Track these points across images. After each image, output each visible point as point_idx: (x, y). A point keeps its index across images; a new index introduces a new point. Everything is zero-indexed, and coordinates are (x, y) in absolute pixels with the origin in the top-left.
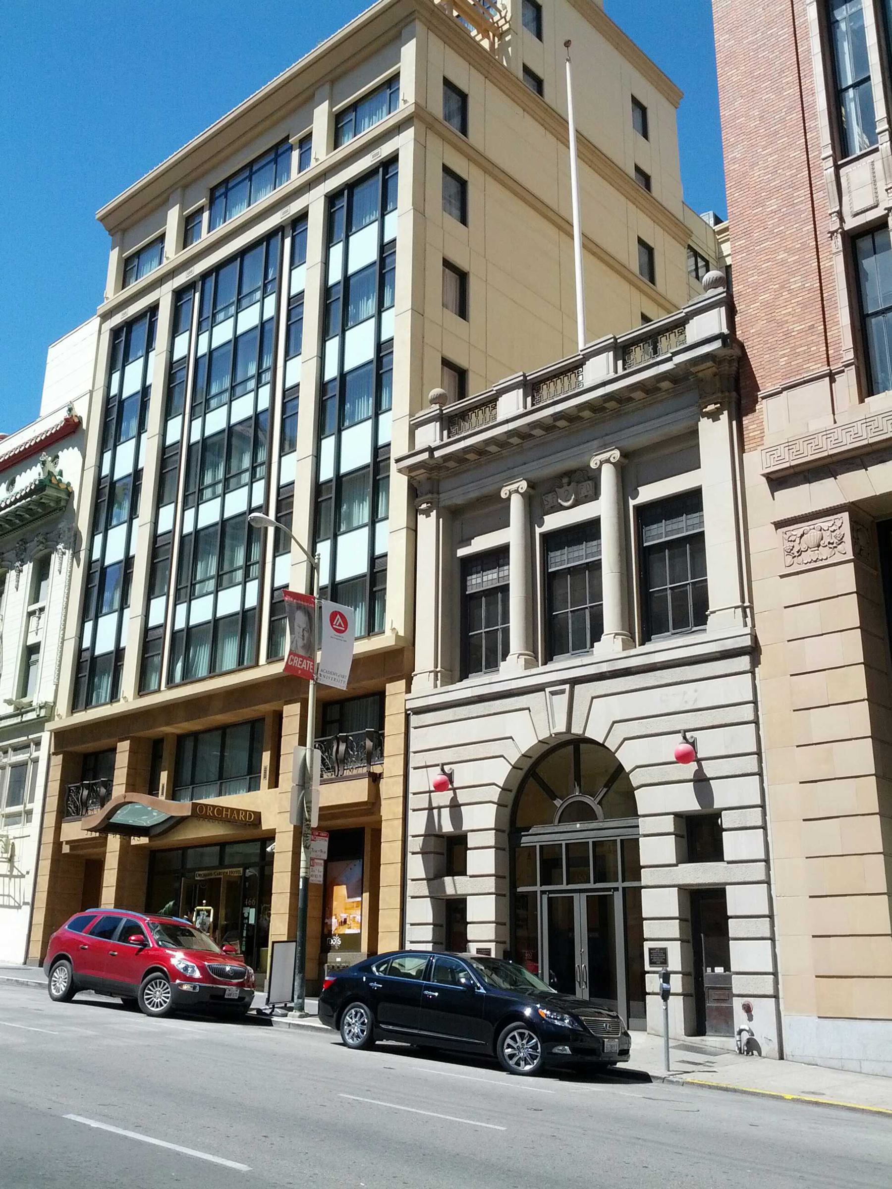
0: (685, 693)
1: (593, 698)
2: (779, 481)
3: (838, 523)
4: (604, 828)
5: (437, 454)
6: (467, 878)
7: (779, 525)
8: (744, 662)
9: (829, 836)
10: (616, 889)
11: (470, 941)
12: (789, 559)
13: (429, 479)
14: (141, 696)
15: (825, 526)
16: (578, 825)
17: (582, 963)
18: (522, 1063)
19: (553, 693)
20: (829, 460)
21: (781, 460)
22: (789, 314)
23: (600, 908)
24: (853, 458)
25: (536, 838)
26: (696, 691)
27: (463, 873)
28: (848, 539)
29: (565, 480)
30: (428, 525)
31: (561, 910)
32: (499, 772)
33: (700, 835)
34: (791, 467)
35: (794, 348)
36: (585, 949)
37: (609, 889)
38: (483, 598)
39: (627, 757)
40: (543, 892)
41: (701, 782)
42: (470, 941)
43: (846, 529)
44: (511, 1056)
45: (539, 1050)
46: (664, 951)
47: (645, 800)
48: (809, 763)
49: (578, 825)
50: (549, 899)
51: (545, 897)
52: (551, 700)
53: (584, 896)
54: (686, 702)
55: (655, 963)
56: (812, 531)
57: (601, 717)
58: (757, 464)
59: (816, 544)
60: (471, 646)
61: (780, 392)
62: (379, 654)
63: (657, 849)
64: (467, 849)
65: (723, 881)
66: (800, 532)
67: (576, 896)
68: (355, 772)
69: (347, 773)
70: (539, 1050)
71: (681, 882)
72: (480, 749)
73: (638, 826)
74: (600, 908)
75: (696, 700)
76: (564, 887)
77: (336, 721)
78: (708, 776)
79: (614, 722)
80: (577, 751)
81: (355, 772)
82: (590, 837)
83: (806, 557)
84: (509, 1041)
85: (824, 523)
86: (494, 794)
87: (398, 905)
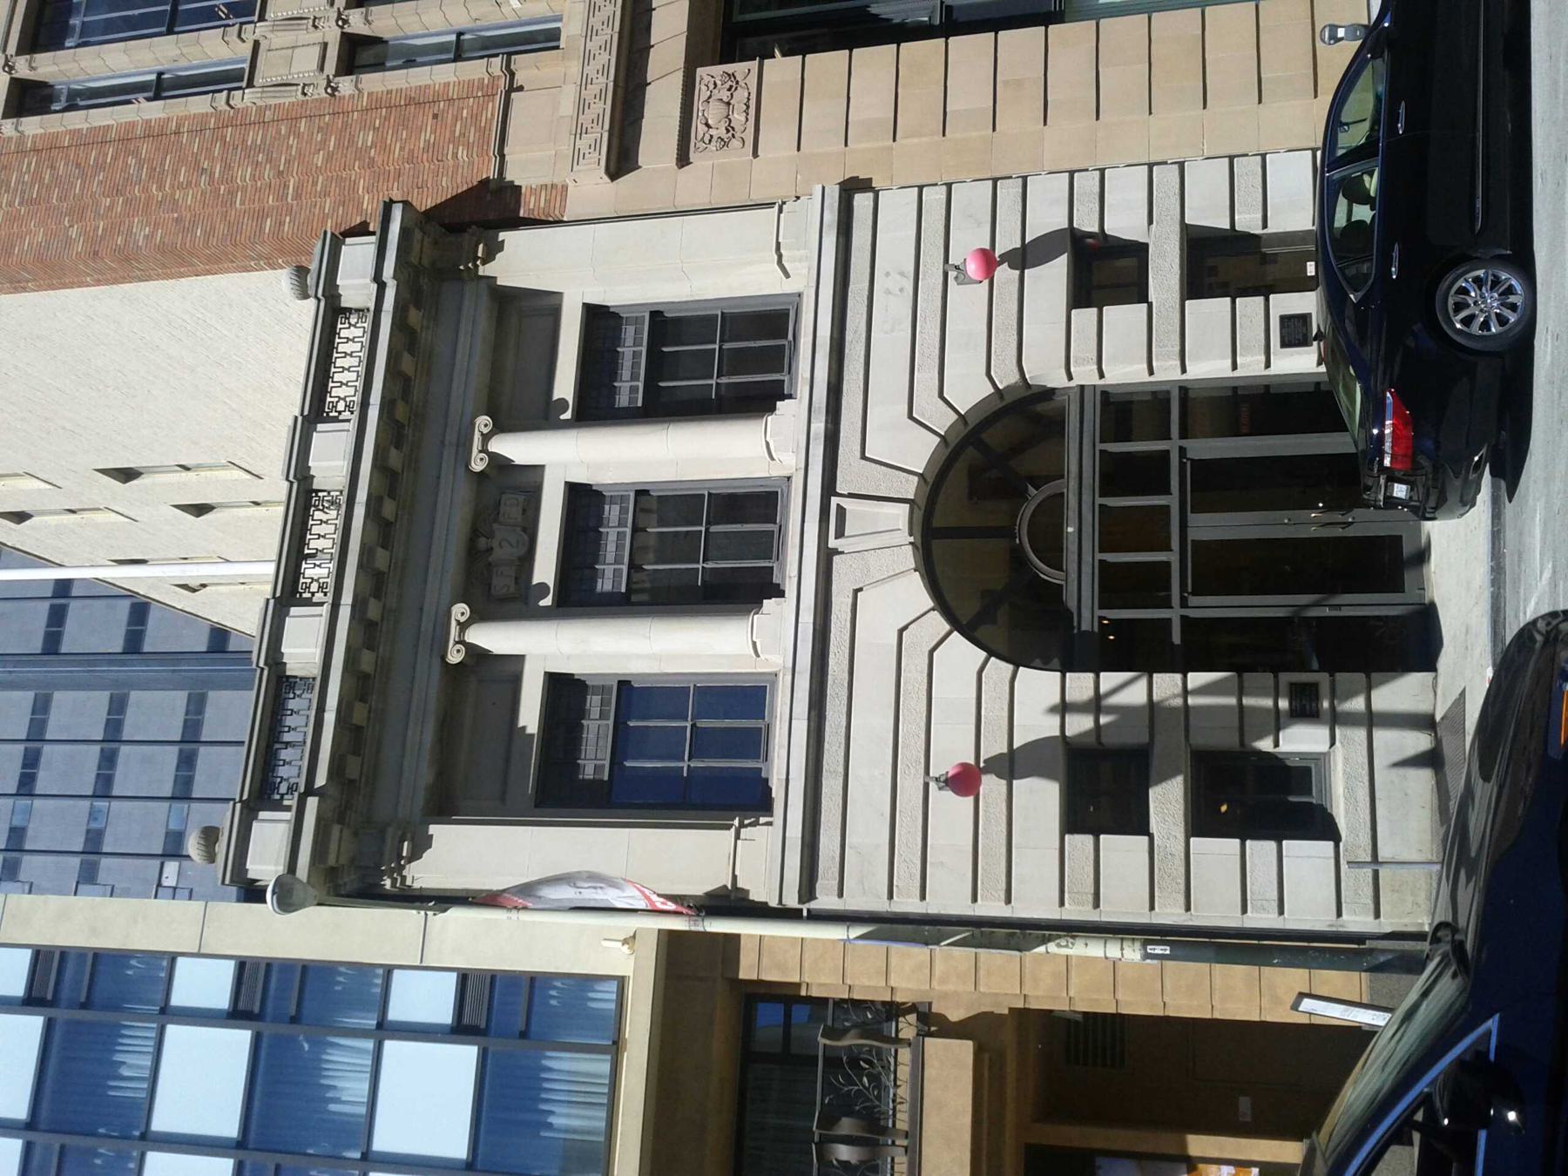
0: (888, 292)
2: (622, 160)
3: (707, 79)
4: (1080, 454)
5: (321, 780)
7: (683, 159)
8: (862, 201)
9: (1122, 78)
10: (1182, 450)
11: (1276, 677)
12: (735, 143)
13: (356, 834)
15: (705, 94)
16: (1070, 530)
17: (1311, 523)
18: (1512, 299)
19: (840, 534)
20: (620, 92)
21: (596, 145)
22: (402, 149)
23: (1217, 484)
24: (629, 59)
25: (1089, 614)
28: (729, 68)
29: (482, 543)
31: (1221, 568)
32: (962, 654)
33: (1103, 271)
35: (452, 140)
36: (1285, 516)
37: (1182, 466)
38: (628, 764)
40: (1184, 603)
41: (1012, 765)
42: (1276, 677)
43: (718, 70)
44: (1502, 320)
45: (1481, 273)
46: (1285, 320)
48: (1019, 116)
49: (1070, 530)
50: (1194, 593)
51: (1194, 600)
53: (1195, 519)
54: (901, 290)
56: (709, 112)
57: (899, 442)
58: (589, 185)
59: (723, 106)
61: (502, 156)
62: (666, 988)
63: (1124, 350)
65: (1177, 228)
66: (702, 128)
67: (1193, 535)
68: (904, 1092)
69: (903, 1123)
70: (1481, 273)
71: (1157, 750)
72: (912, 698)
73: (1082, 387)
74: (1217, 484)
75: (902, 274)
76: (1173, 557)
77: (788, 1015)
78: (1018, 245)
79: (911, 416)
81: (904, 1092)
82: (1092, 500)
83: (738, 117)
84: (1475, 329)
85: (702, 91)
86: (999, 669)
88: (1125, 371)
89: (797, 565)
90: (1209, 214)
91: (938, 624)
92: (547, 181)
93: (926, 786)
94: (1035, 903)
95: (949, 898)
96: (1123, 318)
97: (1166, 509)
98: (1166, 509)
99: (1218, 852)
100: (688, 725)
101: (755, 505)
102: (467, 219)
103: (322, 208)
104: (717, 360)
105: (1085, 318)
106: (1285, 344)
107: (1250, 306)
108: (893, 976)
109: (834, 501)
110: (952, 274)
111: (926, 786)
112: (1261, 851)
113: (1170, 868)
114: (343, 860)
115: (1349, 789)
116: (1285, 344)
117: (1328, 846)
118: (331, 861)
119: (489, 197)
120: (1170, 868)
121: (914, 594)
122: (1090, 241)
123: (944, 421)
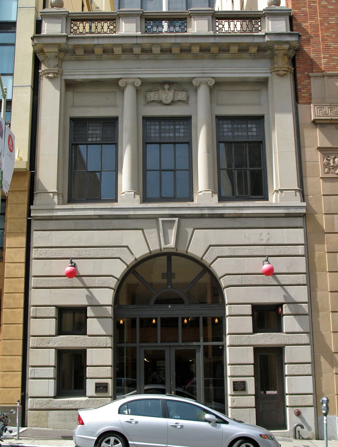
0: (261, 234)
1: (194, 229)
6: (87, 337)
14: (165, 383)
22: (328, 36)
26: (269, 234)
27: (85, 334)
30: (51, 94)
32: (119, 269)
34: (331, 120)
35: (331, 56)
39: (219, 268)
46: (244, 383)
47: (229, 295)
52: (304, 225)
55: (237, 390)
57: (200, 243)
60: (85, 183)
63: (237, 324)
64: (87, 318)
65: (283, 343)
75: (268, 239)
79: (210, 246)
80: (169, 260)
86: (113, 283)
87: (20, 352)
88: (230, 325)
89: (154, 208)
90: (288, 355)
91: (130, 260)
92: (313, 96)
93: (265, 256)
94: (35, 297)
95: (36, 268)
96: (248, 323)
97: (177, 341)
98: (177, 341)
99: (51, 358)
100: (248, 168)
101: (258, 189)
102: (297, 65)
103: (304, 7)
104: (244, 170)
105: (248, 310)
106: (97, 384)
107: (250, 370)
108: (9, 249)
109: (177, 219)
110: (265, 258)
111: (265, 256)
112: (51, 372)
113: (44, 342)
114: (47, 54)
115: (71, 402)
116: (97, 384)
117: (52, 394)
118: (45, 50)
119: (306, 73)
120: (44, 342)
121: (140, 251)
122: (280, 310)
123: (207, 259)
